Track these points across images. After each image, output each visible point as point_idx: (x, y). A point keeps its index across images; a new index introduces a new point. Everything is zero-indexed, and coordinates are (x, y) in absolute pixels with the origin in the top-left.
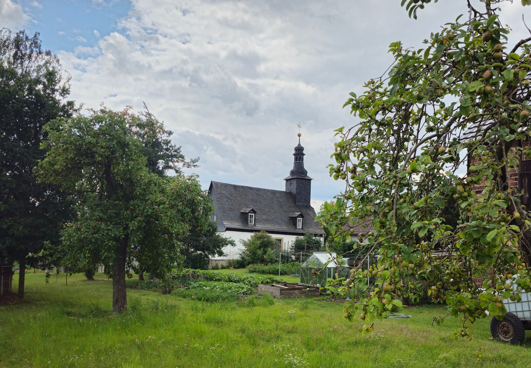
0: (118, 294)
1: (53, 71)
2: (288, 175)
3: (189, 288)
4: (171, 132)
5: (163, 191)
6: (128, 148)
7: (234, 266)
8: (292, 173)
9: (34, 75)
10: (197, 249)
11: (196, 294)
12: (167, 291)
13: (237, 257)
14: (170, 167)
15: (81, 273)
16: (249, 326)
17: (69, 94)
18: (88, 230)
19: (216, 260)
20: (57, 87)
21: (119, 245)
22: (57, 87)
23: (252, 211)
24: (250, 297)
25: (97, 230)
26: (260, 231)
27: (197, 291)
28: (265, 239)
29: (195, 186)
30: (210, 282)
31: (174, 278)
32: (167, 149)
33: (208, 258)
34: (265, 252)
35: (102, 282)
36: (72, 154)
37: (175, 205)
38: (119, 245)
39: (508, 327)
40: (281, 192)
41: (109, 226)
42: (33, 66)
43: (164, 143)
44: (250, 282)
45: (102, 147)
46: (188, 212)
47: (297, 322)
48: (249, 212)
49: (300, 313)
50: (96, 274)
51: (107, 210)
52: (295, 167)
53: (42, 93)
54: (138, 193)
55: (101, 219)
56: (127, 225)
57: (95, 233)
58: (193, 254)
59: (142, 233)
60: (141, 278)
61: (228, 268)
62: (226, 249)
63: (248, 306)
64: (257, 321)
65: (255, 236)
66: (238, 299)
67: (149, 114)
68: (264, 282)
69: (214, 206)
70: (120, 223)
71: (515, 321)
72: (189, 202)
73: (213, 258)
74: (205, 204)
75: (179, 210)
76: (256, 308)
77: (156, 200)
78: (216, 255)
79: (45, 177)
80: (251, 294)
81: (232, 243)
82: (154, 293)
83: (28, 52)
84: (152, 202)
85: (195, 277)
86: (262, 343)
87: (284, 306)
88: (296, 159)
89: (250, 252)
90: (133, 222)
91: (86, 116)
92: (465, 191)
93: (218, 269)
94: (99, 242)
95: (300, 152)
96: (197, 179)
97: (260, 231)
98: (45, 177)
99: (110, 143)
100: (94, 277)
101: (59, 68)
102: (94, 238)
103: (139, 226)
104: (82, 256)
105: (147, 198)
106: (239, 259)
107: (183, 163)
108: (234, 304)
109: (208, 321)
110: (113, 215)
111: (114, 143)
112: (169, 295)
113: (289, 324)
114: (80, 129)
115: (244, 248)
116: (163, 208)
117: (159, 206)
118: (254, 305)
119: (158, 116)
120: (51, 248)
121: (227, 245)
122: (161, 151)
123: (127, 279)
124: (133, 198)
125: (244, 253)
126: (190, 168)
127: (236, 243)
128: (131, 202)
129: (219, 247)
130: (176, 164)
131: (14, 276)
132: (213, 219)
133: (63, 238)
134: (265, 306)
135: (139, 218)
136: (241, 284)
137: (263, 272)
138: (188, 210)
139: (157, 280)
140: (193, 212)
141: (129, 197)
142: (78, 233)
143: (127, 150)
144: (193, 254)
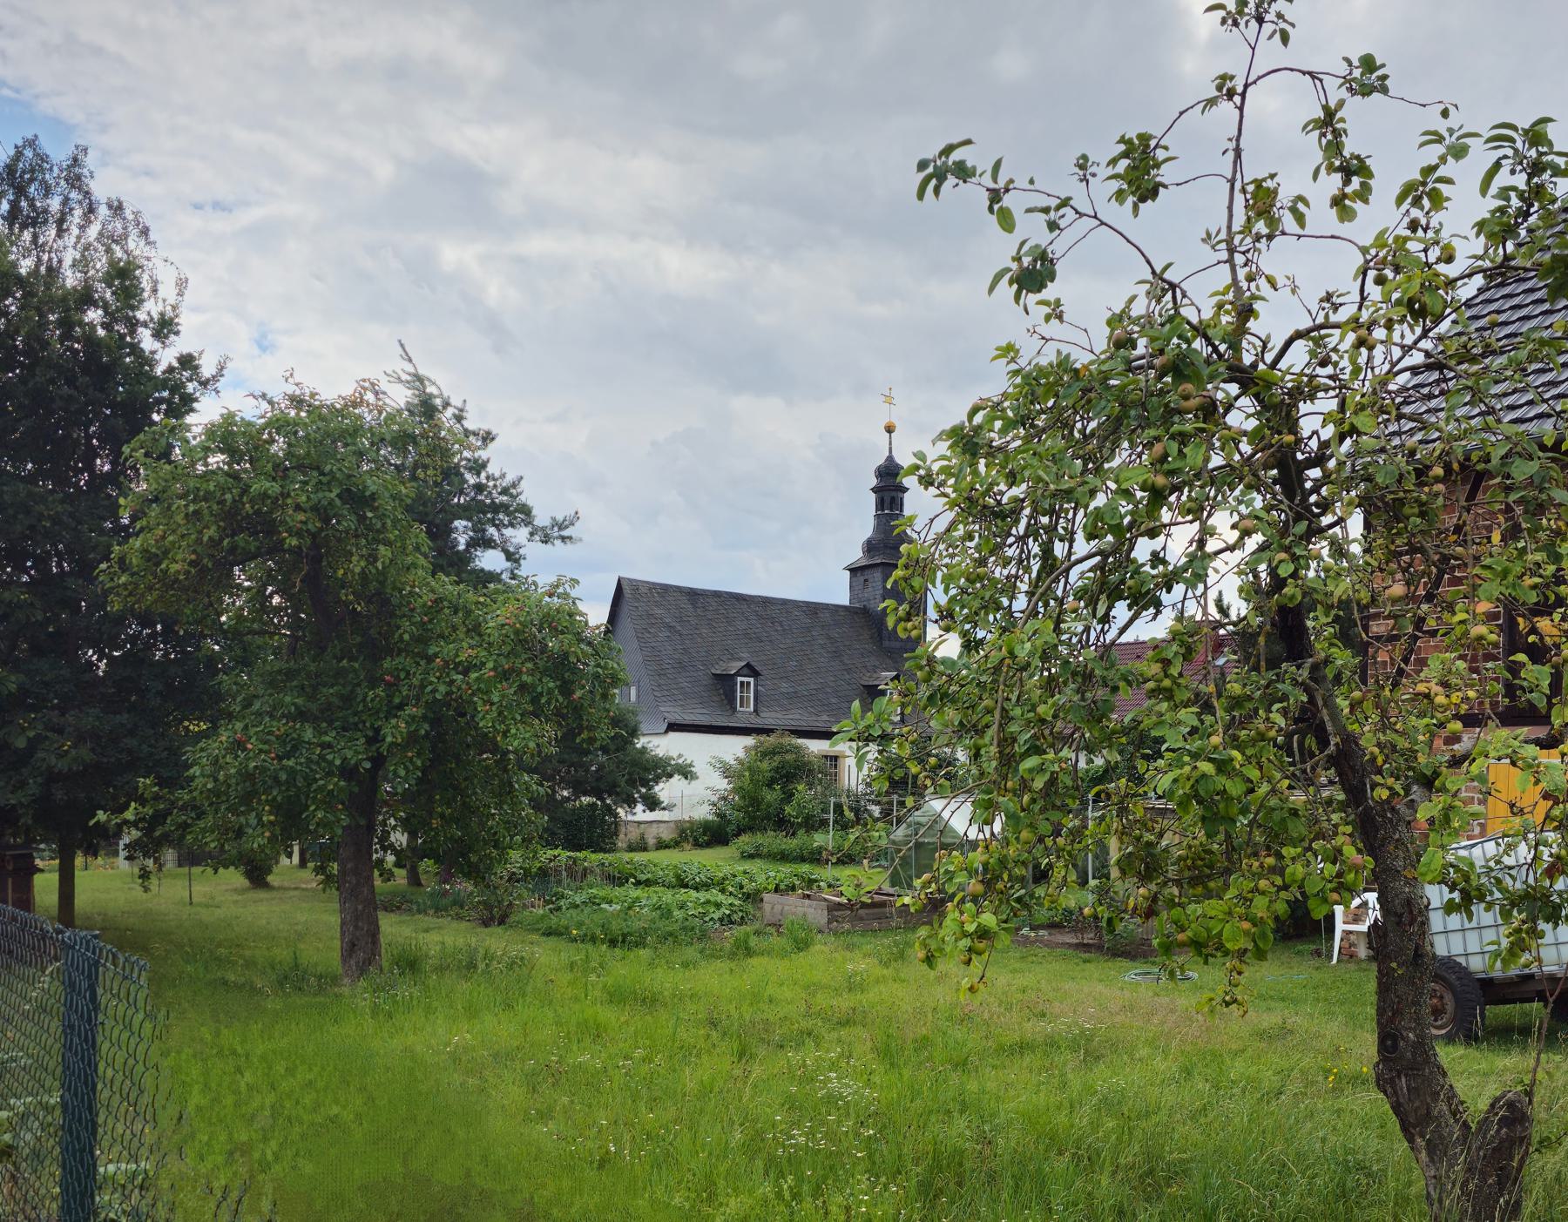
0: (356, 927)
1: (128, 263)
2: (856, 555)
3: (559, 909)
4: (488, 433)
5: (476, 630)
6: (374, 509)
7: (696, 840)
8: (870, 547)
9: (71, 279)
10: (579, 790)
11: (580, 925)
12: (495, 916)
13: (703, 813)
14: (488, 544)
15: (232, 868)
16: (732, 1008)
17: (177, 333)
18: (266, 747)
19: (639, 823)
20: (141, 315)
21: (356, 790)
22: (141, 315)
23: (746, 671)
24: (739, 931)
25: (293, 747)
26: (772, 731)
27: (582, 917)
28: (788, 757)
29: (570, 615)
30: (618, 891)
31: (512, 878)
32: (479, 488)
33: (616, 815)
34: (789, 796)
35: (296, 893)
36: (214, 528)
37: (512, 670)
38: (356, 790)
39: (1442, 997)
40: (837, 608)
41: (326, 733)
42: (70, 255)
43: (470, 469)
44: (741, 887)
45: (298, 508)
46: (550, 692)
47: (872, 995)
48: (738, 674)
49: (879, 971)
50: (275, 869)
51: (315, 688)
52: (877, 528)
53: (101, 332)
54: (406, 637)
55: (301, 715)
56: (377, 730)
57: (288, 756)
58: (570, 805)
59: (419, 755)
60: (414, 880)
61: (675, 844)
62: (666, 790)
63: (732, 956)
64: (755, 998)
65: (756, 747)
66: (704, 936)
67: (419, 379)
68: (782, 887)
69: (628, 658)
70: (356, 724)
71: (1459, 979)
72: (554, 663)
73: (630, 818)
74: (598, 665)
75: (523, 687)
76: (754, 961)
77: (457, 655)
78: (640, 807)
79: (130, 594)
80: (742, 921)
81: (686, 772)
82: (455, 924)
83: (55, 204)
84: (447, 663)
85: (579, 875)
86: (762, 1051)
87: (836, 955)
88: (880, 505)
89: (743, 797)
90: (394, 721)
91: (248, 418)
92: (1166, 676)
93: (645, 849)
94: (300, 782)
95: (890, 481)
96: (574, 593)
97: (772, 731)
98: (130, 594)
99: (320, 495)
100: (270, 878)
101: (147, 251)
102: (283, 768)
103: (409, 733)
104: (253, 822)
105: (431, 652)
106: (710, 818)
107: (530, 529)
108: (691, 952)
109: (616, 997)
110: (335, 700)
111: (333, 495)
112: (499, 930)
113: (845, 1003)
114: (233, 453)
115: (723, 784)
116: (477, 679)
117: (465, 673)
118: (749, 952)
119: (445, 384)
120: (156, 798)
121: (670, 776)
122: (461, 492)
123: (378, 882)
124: (391, 652)
125: (724, 799)
126: (549, 546)
127: (700, 770)
128: (387, 664)
129: (645, 783)
130: (508, 532)
131: (38, 879)
132: (629, 697)
133: (196, 770)
134: (783, 954)
135: (411, 710)
136: (714, 895)
137: (783, 857)
138: (551, 685)
139: (465, 886)
140: (566, 689)
141: (376, 650)
142: (237, 756)
143: (370, 515)
144: (570, 805)
